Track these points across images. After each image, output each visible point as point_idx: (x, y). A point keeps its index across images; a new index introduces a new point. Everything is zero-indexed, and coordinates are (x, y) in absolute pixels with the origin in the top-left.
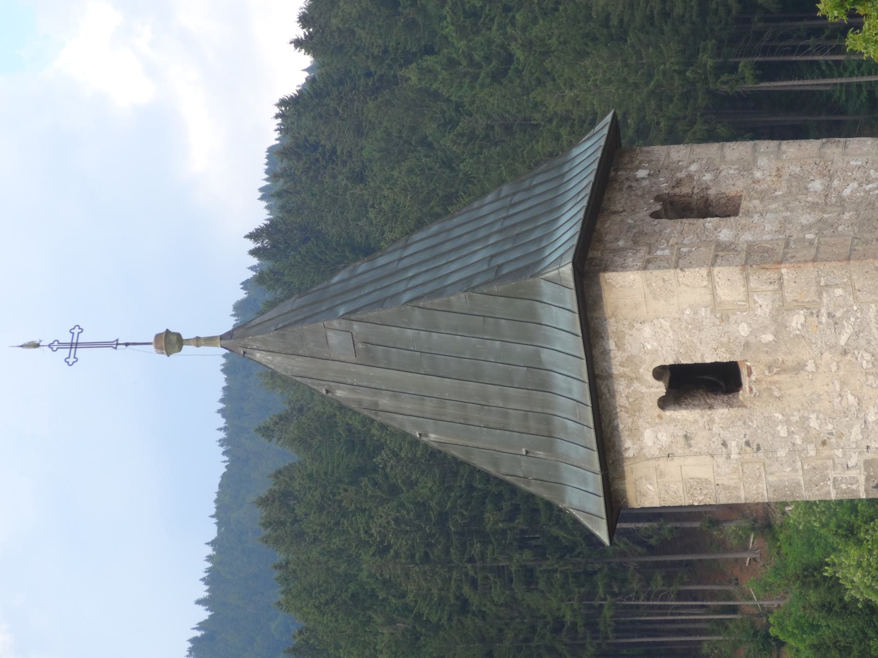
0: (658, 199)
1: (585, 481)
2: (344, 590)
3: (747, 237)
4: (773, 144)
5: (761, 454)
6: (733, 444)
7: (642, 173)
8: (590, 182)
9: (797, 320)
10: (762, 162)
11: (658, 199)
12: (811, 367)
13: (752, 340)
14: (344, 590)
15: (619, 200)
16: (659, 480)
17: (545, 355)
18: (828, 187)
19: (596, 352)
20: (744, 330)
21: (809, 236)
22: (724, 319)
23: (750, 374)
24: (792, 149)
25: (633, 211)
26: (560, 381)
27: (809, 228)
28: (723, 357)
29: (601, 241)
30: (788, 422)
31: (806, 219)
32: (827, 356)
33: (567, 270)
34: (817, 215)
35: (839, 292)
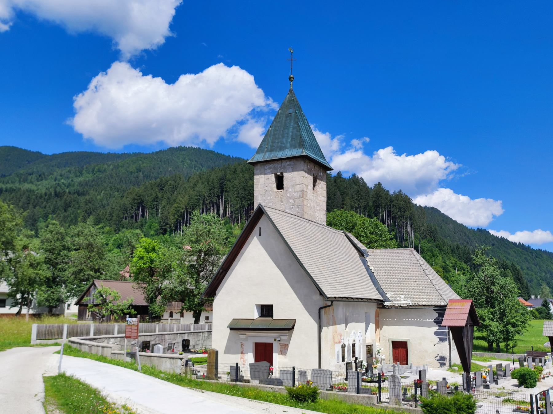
0: (317, 176)
1: (260, 158)
2: (22, 180)
3: (309, 192)
4: (326, 201)
5: (264, 194)
6: (266, 188)
7: (321, 173)
8: (323, 157)
9: (292, 201)
10: (323, 198)
11: (317, 176)
12: (282, 204)
13: (288, 192)
14: (22, 180)
15: (317, 168)
16: (92, 336)
17: (287, 150)
18: (317, 210)
19: (287, 160)
20: (290, 190)
21: (309, 205)
22: (293, 186)
23: (281, 192)
24: (325, 204)
25: (315, 170)
26: (281, 153)
27: (310, 205)
28: (284, 186)
29: (309, 163)
30: (270, 199)
31: (312, 204)
32: (284, 207)
33: (305, 154)
34: (313, 207)
35: (297, 210)
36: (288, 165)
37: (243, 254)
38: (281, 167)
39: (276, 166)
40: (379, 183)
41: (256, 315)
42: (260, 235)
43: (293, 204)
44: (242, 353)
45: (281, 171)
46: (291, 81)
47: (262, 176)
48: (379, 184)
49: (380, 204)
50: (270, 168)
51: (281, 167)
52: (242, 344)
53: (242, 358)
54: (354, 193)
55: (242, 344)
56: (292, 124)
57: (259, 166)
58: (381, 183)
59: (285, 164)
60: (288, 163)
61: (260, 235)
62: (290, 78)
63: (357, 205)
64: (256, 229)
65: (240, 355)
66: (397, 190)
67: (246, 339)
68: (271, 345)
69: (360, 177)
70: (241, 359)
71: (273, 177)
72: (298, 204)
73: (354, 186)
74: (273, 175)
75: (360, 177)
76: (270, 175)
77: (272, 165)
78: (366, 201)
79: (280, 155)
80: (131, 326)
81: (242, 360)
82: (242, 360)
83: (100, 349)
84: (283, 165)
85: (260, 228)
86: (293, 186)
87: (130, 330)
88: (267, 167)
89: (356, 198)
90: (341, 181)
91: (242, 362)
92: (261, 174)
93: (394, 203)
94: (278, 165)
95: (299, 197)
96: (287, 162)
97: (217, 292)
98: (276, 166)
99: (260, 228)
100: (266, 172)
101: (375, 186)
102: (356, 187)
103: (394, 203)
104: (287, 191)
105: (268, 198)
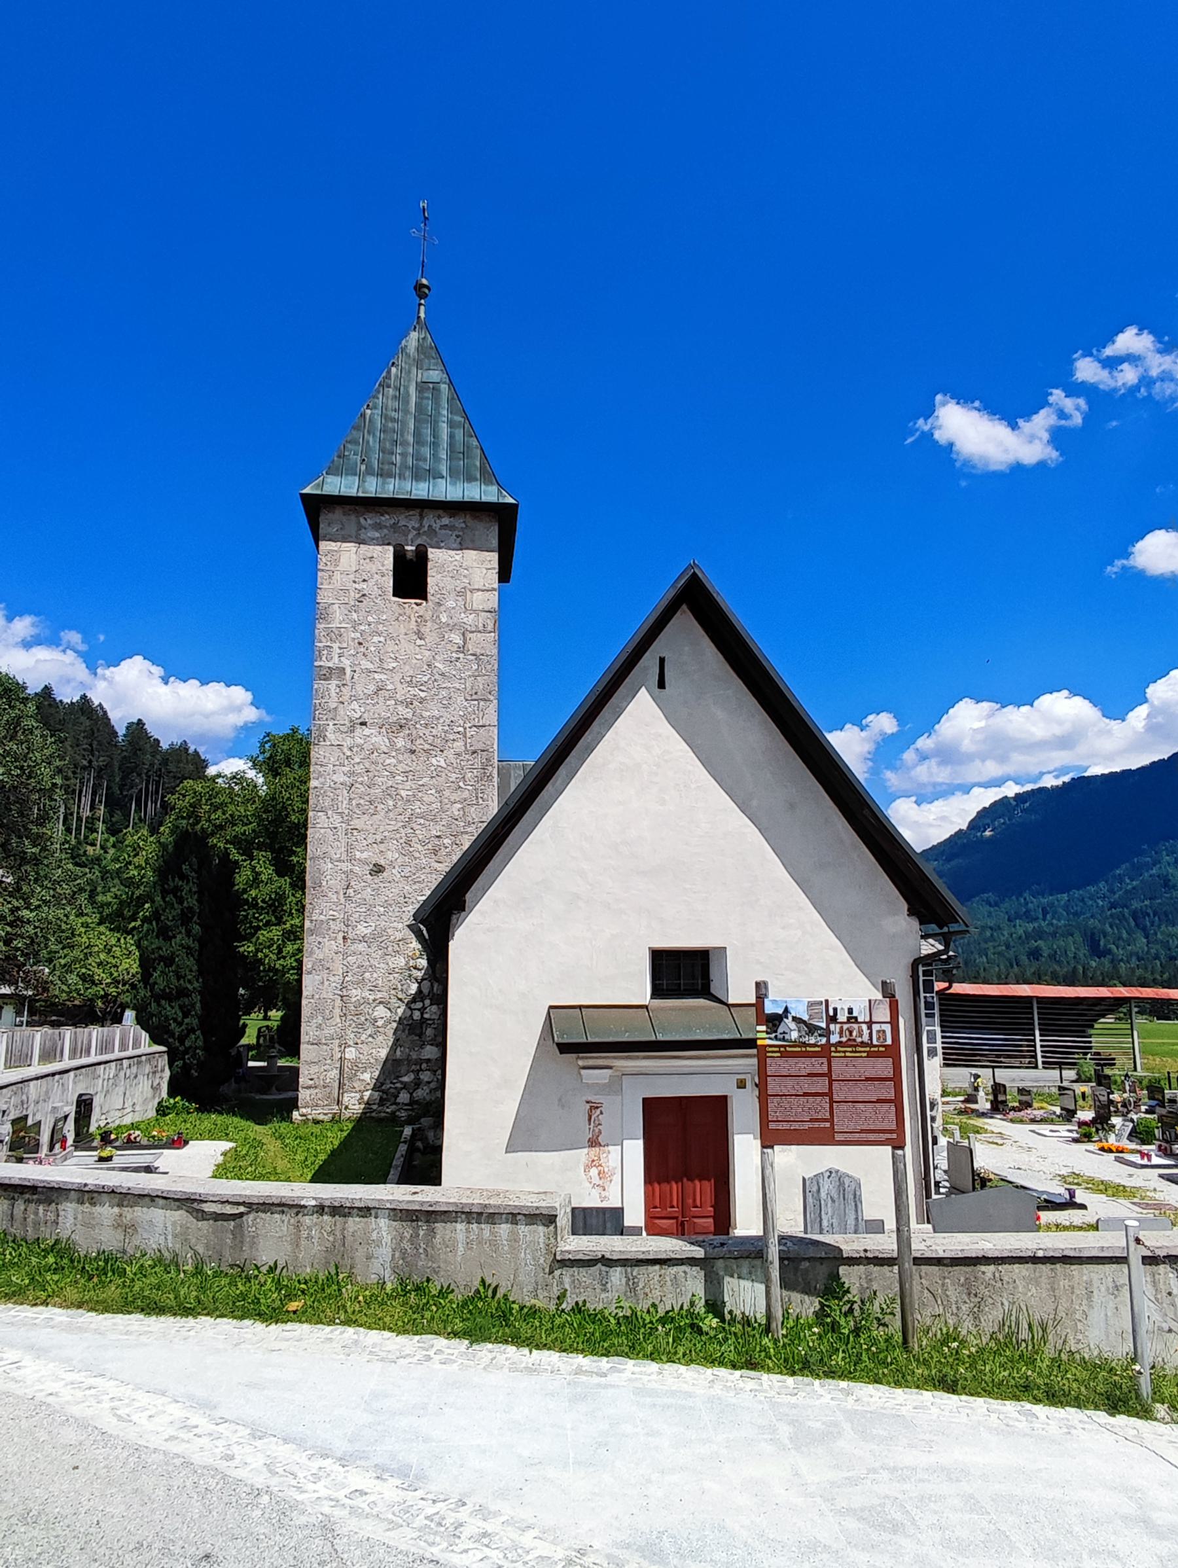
9: (458, 640)
12: (419, 642)
13: (442, 608)
19: (441, 512)
20: (451, 603)
23: (417, 604)
28: (431, 589)
36: (443, 527)
37: (590, 749)
38: (418, 529)
39: (402, 523)
40: (140, 720)
41: (639, 989)
42: (661, 685)
43: (462, 649)
44: (594, 1143)
45: (419, 541)
46: (422, 296)
47: (351, 546)
48: (140, 723)
49: (137, 766)
50: (378, 527)
51: (418, 529)
52: (594, 1107)
53: (592, 1163)
54: (82, 735)
55: (594, 1107)
56: (445, 412)
57: (338, 514)
58: (145, 721)
59: (431, 520)
60: (446, 521)
61: (661, 685)
62: (419, 287)
63: (85, 763)
64: (649, 661)
65: (583, 1155)
66: (178, 741)
67: (614, 1087)
68: (719, 1105)
69: (96, 703)
70: (587, 1168)
71: (387, 556)
72: (478, 651)
73: (83, 719)
74: (391, 548)
75: (96, 703)
76: (379, 548)
77: (386, 519)
78: (108, 756)
79: (420, 490)
80: (826, 1052)
81: (594, 1172)
82: (594, 1172)
83: (383, 1228)
84: (426, 523)
85: (662, 661)
86: (461, 593)
87: (821, 1085)
88: (369, 520)
89: (85, 747)
90: (50, 705)
91: (596, 1180)
92: (345, 540)
93: (171, 767)
94: (410, 521)
95: (481, 628)
96: (439, 517)
97: (468, 896)
98: (402, 523)
99: (662, 661)
100: (363, 536)
101: (130, 726)
102: (88, 723)
103: (171, 767)
104: (439, 604)
105: (370, 619)
